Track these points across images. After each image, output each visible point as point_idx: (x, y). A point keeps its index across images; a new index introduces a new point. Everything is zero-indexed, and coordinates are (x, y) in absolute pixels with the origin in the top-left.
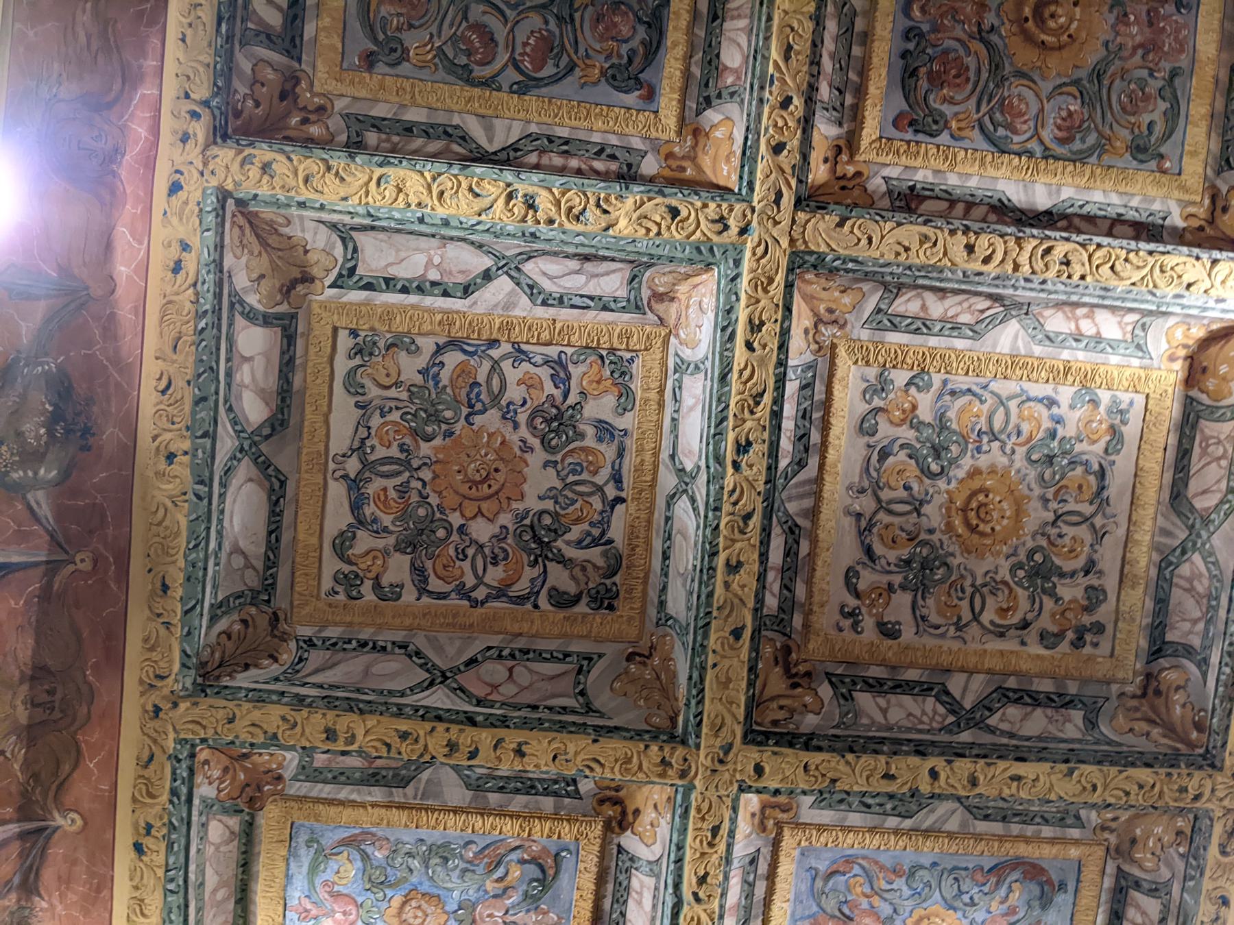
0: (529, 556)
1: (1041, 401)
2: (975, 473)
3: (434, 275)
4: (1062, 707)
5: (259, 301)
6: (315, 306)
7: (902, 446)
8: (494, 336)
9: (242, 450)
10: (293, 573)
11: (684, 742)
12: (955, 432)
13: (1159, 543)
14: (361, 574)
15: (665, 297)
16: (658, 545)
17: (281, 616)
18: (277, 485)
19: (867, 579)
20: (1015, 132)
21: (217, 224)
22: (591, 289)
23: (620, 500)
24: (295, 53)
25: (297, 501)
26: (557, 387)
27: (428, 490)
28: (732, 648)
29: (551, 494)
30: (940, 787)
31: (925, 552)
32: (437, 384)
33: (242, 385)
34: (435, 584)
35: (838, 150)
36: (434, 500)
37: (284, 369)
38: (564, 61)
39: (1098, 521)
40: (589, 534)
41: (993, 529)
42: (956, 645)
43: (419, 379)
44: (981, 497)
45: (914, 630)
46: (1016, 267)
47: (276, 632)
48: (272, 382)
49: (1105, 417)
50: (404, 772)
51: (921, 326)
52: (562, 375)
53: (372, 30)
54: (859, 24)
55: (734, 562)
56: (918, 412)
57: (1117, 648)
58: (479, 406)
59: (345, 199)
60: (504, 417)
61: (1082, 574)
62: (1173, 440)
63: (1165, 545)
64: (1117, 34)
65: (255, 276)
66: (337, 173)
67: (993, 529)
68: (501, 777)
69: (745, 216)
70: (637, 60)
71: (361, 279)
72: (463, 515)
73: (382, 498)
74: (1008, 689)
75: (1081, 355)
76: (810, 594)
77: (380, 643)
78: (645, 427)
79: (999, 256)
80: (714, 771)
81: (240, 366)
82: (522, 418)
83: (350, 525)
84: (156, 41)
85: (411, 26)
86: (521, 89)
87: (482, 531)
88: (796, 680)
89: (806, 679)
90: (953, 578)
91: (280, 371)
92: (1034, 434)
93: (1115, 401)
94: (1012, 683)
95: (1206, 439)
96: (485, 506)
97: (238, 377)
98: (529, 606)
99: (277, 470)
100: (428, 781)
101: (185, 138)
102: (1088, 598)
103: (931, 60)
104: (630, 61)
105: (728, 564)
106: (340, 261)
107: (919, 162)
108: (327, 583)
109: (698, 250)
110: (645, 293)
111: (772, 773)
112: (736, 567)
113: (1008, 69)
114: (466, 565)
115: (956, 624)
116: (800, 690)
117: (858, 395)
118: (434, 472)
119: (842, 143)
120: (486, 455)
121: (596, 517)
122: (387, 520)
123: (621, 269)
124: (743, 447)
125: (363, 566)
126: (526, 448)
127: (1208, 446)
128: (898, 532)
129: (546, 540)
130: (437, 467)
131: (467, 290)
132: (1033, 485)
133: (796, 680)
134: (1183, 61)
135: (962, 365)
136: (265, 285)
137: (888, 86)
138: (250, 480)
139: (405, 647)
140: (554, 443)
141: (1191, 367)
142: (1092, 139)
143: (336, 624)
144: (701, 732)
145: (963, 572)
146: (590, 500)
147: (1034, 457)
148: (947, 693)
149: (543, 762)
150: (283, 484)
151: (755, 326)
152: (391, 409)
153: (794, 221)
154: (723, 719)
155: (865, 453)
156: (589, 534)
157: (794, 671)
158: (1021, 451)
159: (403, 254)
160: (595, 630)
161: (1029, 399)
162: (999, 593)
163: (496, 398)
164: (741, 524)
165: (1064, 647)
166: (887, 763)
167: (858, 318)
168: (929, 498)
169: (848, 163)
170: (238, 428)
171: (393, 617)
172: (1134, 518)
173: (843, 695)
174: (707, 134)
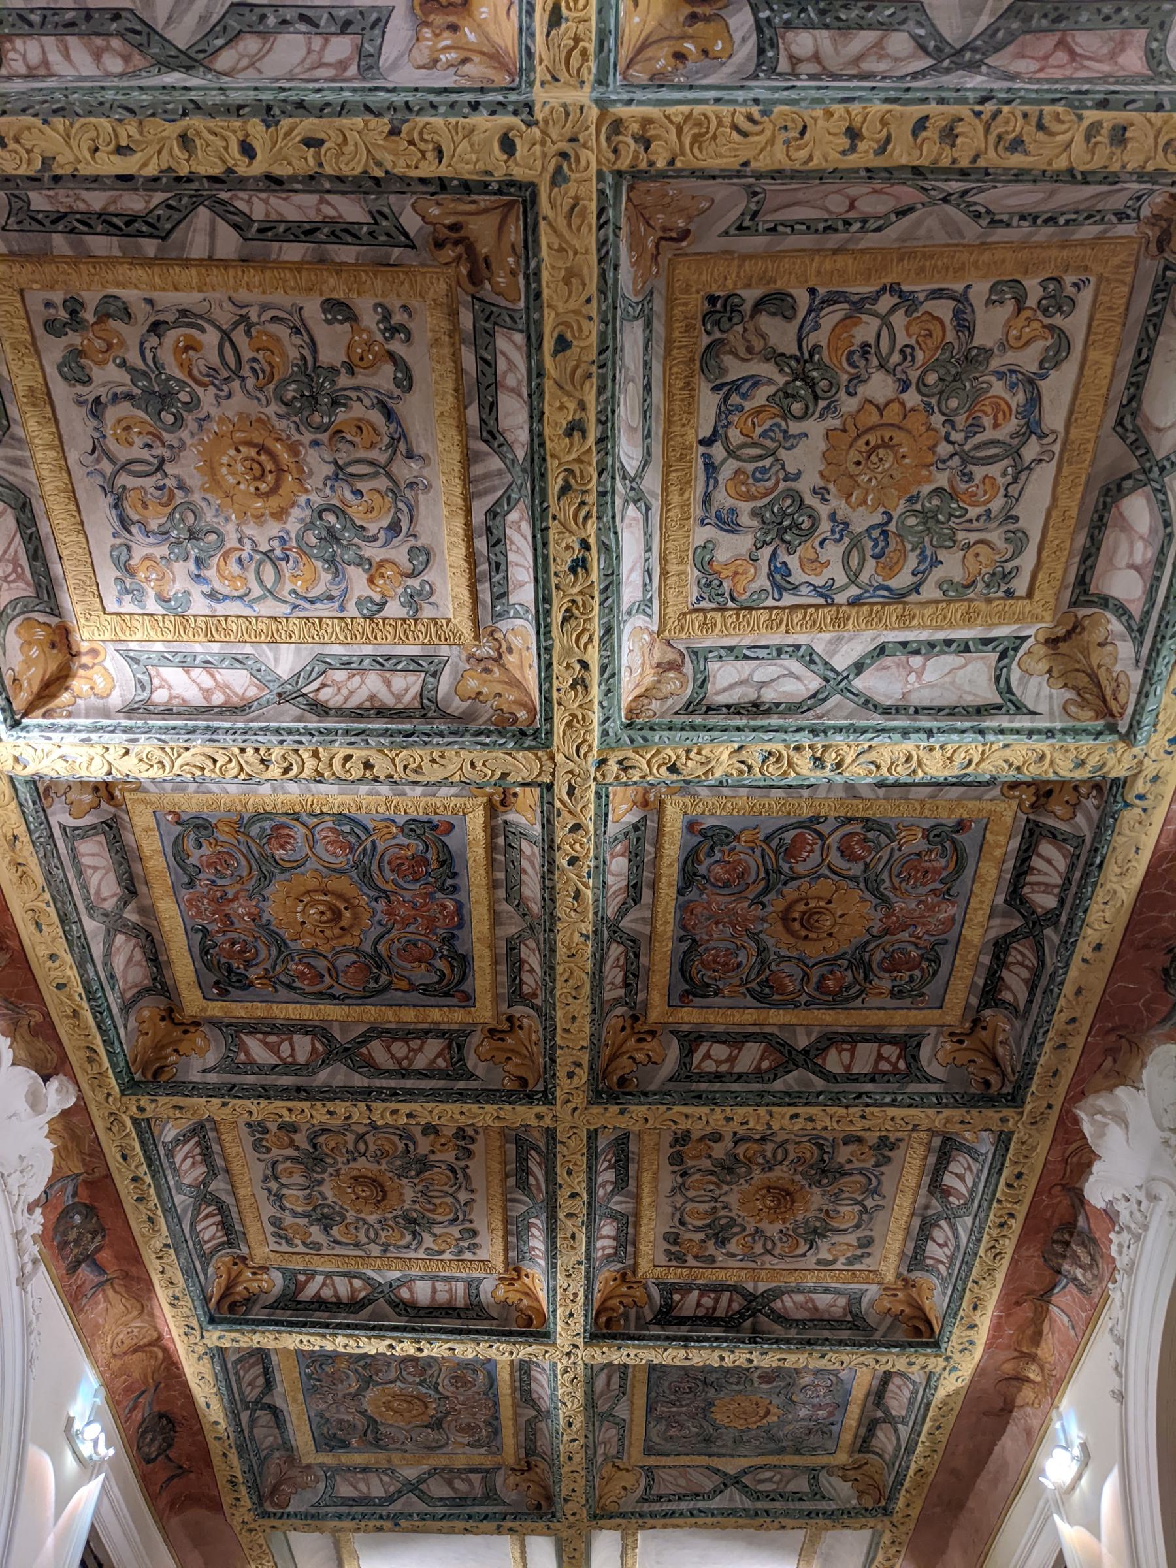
0: (821, 359)
1: (226, 597)
2: (280, 514)
3: (916, 661)
4: (66, 214)
5: (1109, 621)
6: (1048, 618)
7: (375, 538)
8: (854, 610)
9: (1162, 469)
10: (1127, 309)
11: (619, 174)
12: (317, 558)
13: (21, 449)
14: (1039, 313)
15: (665, 667)
16: (657, 395)
17: (1153, 248)
18: (1127, 421)
19: (384, 378)
20: (331, 829)
21: (1141, 715)
22: (746, 667)
23: (707, 442)
24: (1031, 825)
25: (1106, 404)
26: (785, 564)
27: (943, 431)
28: (568, 325)
29: (789, 440)
30: (234, 132)
31: (316, 418)
32: (923, 552)
33: (1147, 542)
34: (944, 309)
35: (503, 803)
36: (937, 419)
37: (1093, 550)
38: (774, 844)
39: (107, 467)
40: (744, 396)
41: (238, 451)
42: (243, 295)
43: (942, 555)
44: (263, 487)
45: (305, 313)
46: (316, 754)
47: (1164, 224)
48: (1111, 537)
49: (145, 585)
50: (1015, 25)
51: (384, 664)
52: (778, 577)
53: (956, 849)
54: (501, 893)
55: (577, 435)
56: (366, 576)
57: (19, 305)
58: (875, 533)
59: (1006, 746)
60: (847, 524)
61: (103, 399)
62: (56, 569)
63: (13, 447)
64: (256, 906)
65: (1109, 648)
66: (1010, 765)
67: (238, 451)
68: (870, 27)
69: (603, 775)
70: (706, 849)
71: (994, 649)
72: (903, 404)
73: (1000, 415)
74: (151, 236)
75: (198, 648)
76: (456, 358)
77: (1027, 224)
78: (681, 532)
79: (337, 762)
80: (573, 140)
81: (1146, 564)
82: (825, 526)
83: (1044, 377)
84: (1162, 842)
85: (919, 854)
86: (816, 820)
87: (880, 386)
88: (455, 235)
89: (441, 237)
90: (271, 387)
91: (1098, 549)
92: (222, 563)
93: (139, 599)
94: (150, 247)
95: (21, 577)
96: (875, 418)
97: (1150, 554)
98: (822, 291)
99: (1124, 439)
100: (979, 13)
101: (1156, 779)
102: (83, 368)
103: (428, 874)
104: (712, 848)
105: (584, 432)
106: (1014, 665)
107: (423, 801)
108: (1085, 298)
109: (645, 739)
110: (688, 668)
111: (487, 142)
112: (573, 429)
113: (354, 874)
114: (902, 339)
115: (250, 326)
116: (447, 222)
117: (438, 587)
118: (934, 453)
119: (502, 809)
120: (870, 480)
121: (735, 418)
122: (998, 388)
123: (718, 693)
124: (579, 565)
125: (1035, 325)
126: (821, 493)
127: (14, 571)
128: (357, 440)
129: (798, 383)
130: (930, 459)
131: (882, 650)
132: (204, 504)
133: (455, 235)
134: (186, 894)
135: (330, 630)
136: (1099, 635)
137: (465, 854)
138: (1158, 430)
139: (993, 222)
140: (789, 502)
141: (69, 646)
142: (255, 831)
143: (1082, 243)
144: (598, 200)
145: (260, 395)
146: (742, 439)
147: (213, 537)
148: (236, 226)
149: (820, 122)
150: (1120, 422)
151: (580, 683)
152: (978, 520)
153: (553, 774)
154: (569, 225)
155: (418, 528)
156: (744, 396)
157: (460, 249)
158: (231, 542)
159: (947, 679)
160: (734, 270)
161: (241, 598)
162: (204, 370)
163: (856, 543)
164: (572, 482)
165: (91, 299)
166: (321, 165)
167: (456, 665)
168: (329, 483)
169: (492, 794)
170: (1161, 496)
171: (1003, 261)
172: (65, 474)
173: (386, 218)
174: (635, 803)
